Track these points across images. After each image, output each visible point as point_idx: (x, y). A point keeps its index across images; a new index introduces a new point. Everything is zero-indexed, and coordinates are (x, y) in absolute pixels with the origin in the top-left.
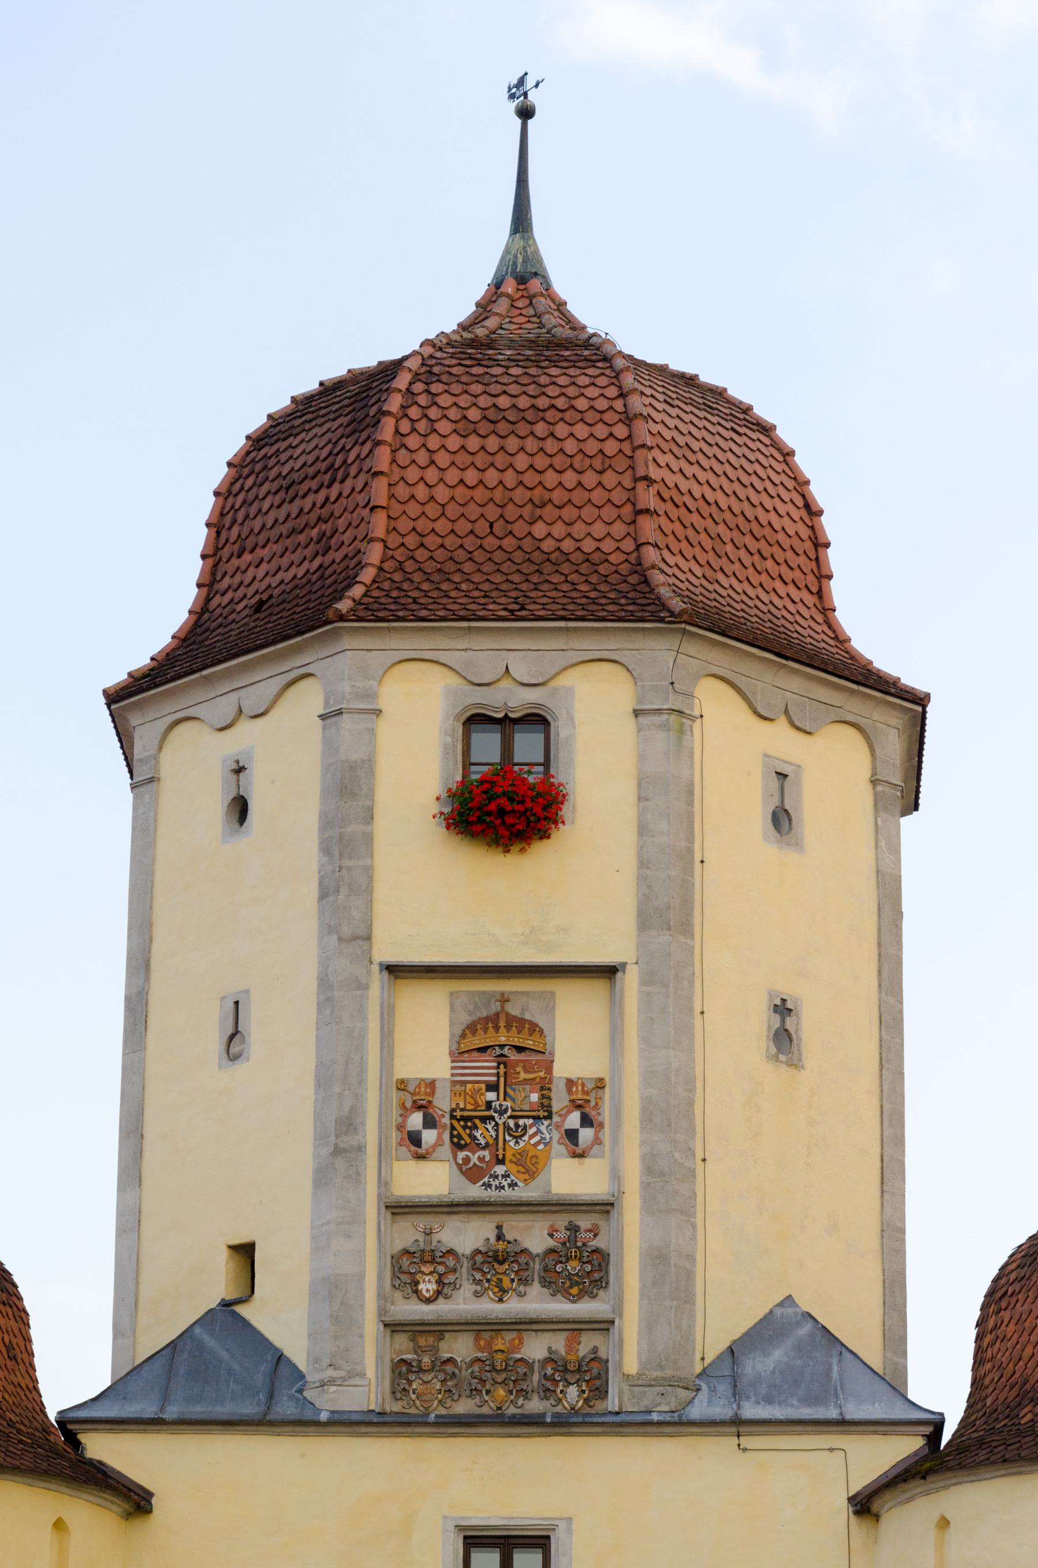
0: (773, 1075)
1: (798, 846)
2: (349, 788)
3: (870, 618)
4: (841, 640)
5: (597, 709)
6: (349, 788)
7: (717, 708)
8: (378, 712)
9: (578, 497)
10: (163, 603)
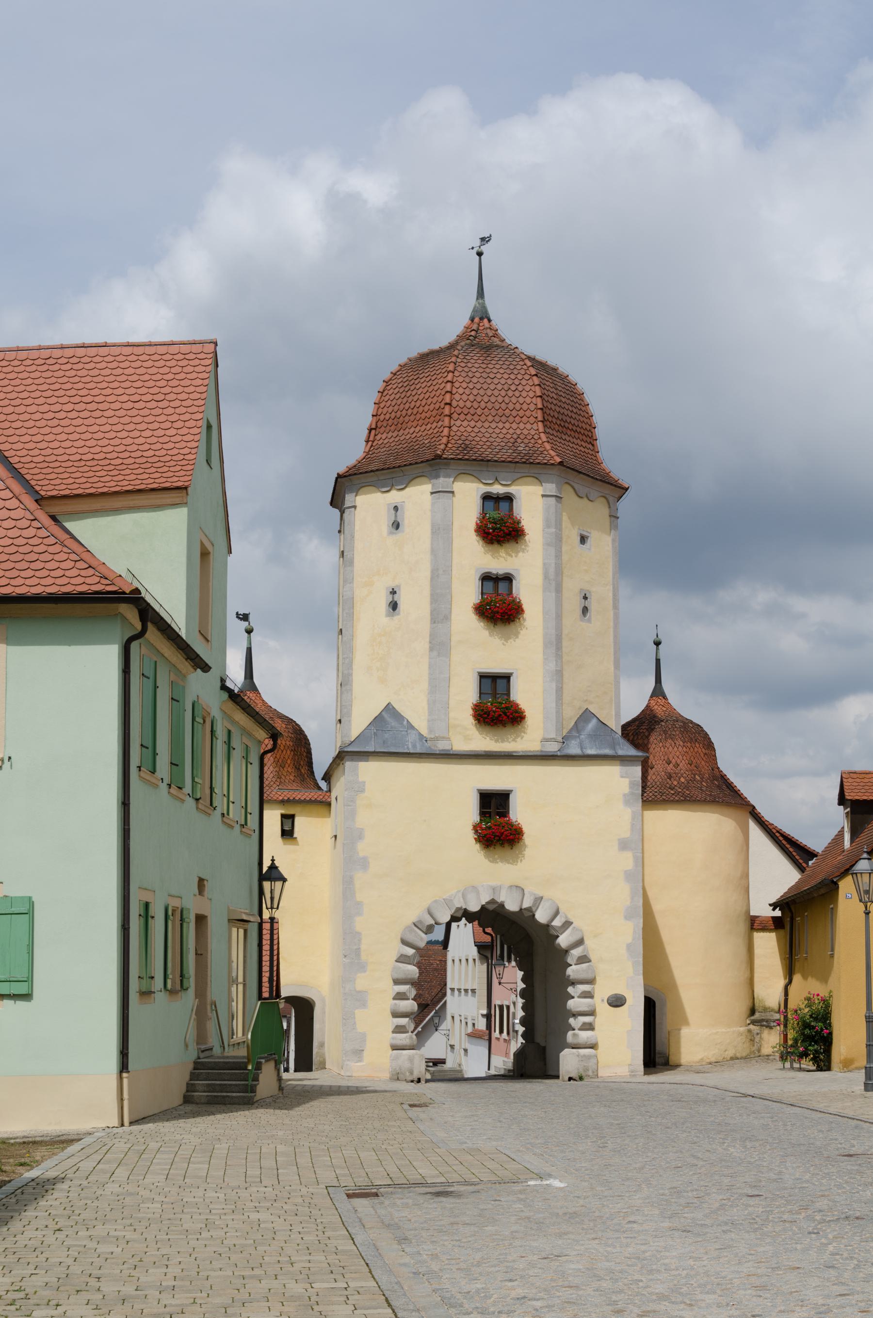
1: (589, 621)
2: (442, 532)
8: (453, 492)
9: (521, 413)
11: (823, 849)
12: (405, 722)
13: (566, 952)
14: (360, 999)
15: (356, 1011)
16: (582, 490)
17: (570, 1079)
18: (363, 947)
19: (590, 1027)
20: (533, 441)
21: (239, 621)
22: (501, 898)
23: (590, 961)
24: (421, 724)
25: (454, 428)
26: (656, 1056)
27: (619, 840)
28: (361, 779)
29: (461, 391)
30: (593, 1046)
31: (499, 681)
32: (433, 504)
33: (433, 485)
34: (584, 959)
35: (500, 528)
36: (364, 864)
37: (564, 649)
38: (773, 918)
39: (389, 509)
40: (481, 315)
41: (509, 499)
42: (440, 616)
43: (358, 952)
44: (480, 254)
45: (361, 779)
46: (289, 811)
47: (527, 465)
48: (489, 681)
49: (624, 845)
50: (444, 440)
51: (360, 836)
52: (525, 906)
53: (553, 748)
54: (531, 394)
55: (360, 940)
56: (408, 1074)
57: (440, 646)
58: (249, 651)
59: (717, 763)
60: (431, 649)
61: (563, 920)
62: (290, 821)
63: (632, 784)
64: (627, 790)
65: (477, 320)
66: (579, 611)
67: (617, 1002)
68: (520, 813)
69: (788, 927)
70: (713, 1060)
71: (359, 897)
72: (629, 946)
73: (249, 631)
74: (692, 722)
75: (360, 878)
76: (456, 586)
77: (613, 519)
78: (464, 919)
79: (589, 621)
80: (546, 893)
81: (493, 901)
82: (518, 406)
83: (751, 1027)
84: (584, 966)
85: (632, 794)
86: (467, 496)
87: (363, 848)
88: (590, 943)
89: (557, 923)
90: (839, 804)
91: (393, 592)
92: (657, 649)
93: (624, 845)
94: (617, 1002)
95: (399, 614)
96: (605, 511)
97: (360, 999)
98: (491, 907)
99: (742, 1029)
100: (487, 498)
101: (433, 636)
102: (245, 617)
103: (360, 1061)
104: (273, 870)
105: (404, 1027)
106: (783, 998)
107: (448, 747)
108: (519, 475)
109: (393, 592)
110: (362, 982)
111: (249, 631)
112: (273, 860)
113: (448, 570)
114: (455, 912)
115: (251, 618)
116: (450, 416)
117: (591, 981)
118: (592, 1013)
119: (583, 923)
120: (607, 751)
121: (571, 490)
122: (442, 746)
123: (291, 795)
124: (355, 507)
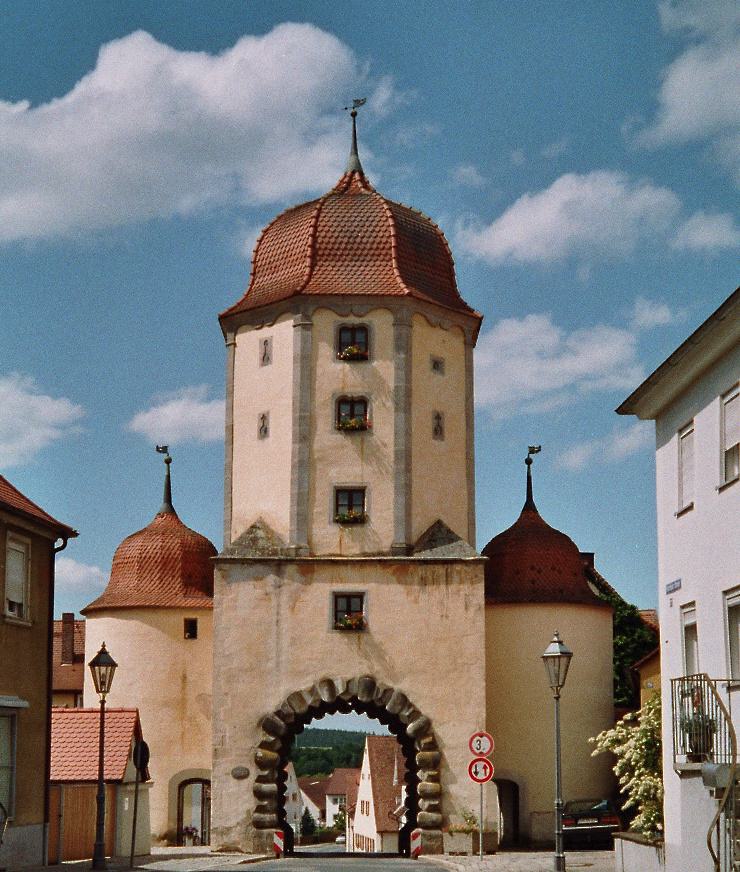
2: (306, 362)
29: (323, 234)
31: (355, 495)
33: (323, 340)
38: (298, 775)
42: (304, 434)
44: (354, 115)
48: (346, 495)
58: (168, 476)
59: (623, 603)
66: (429, 431)
68: (372, 614)
73: (168, 461)
78: (369, 700)
91: (264, 418)
92: (529, 467)
96: (461, 347)
100: (343, 329)
102: (165, 450)
109: (264, 418)
111: (168, 461)
112: (104, 646)
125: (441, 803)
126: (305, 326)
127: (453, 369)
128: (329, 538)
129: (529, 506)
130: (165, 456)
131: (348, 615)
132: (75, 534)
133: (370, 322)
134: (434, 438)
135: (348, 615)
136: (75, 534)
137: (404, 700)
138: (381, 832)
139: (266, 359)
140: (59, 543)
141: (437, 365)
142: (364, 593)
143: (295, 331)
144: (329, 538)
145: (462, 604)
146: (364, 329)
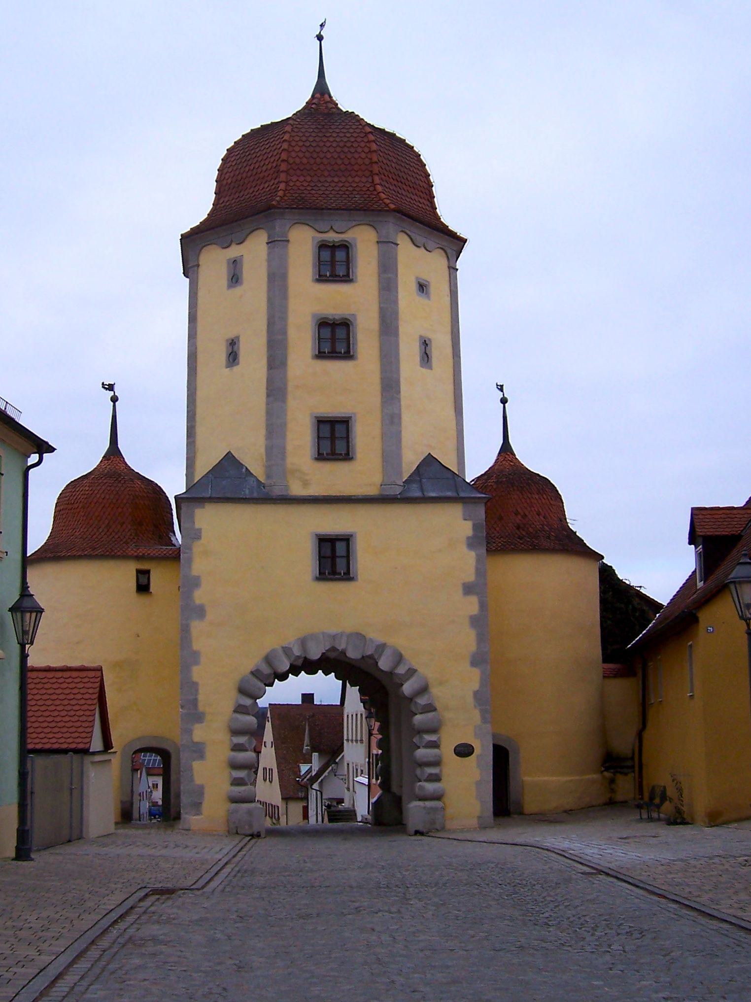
0: (428, 335)
2: (277, 281)
3: (450, 210)
4: (438, 218)
5: (364, 242)
6: (277, 281)
7: (403, 242)
8: (288, 241)
10: (199, 205)
11: (668, 601)
12: (244, 470)
13: (411, 700)
14: (199, 751)
15: (194, 763)
16: (419, 239)
17: (417, 833)
18: (201, 697)
19: (436, 778)
20: (368, 193)
21: (104, 390)
22: (341, 646)
23: (435, 710)
24: (257, 469)
25: (291, 184)
26: (505, 803)
27: (464, 584)
28: (197, 526)
30: (438, 797)
31: (338, 427)
32: (269, 254)
34: (430, 708)
35: (334, 265)
36: (200, 612)
37: (402, 393)
39: (228, 263)
40: (321, 89)
41: (345, 247)
43: (195, 703)
45: (197, 526)
46: (144, 566)
47: (368, 209)
49: (468, 589)
50: (280, 193)
51: (195, 583)
52: (369, 653)
53: (397, 491)
54: (366, 150)
55: (197, 690)
56: (247, 827)
57: (276, 391)
60: (268, 396)
61: (407, 668)
62: (147, 576)
63: (475, 527)
64: (470, 532)
65: (318, 95)
67: (464, 751)
69: (640, 675)
70: (568, 807)
71: (196, 646)
72: (476, 694)
73: (114, 399)
74: (538, 475)
75: (197, 627)
76: (292, 333)
77: (452, 270)
79: (431, 368)
80: (391, 641)
81: (333, 649)
82: (353, 161)
83: (606, 773)
84: (430, 715)
85: (475, 536)
86: (302, 242)
87: (199, 596)
88: (436, 691)
89: (401, 670)
90: (690, 543)
93: (468, 589)
94: (464, 751)
95: (238, 364)
96: (444, 262)
97: (199, 751)
98: (332, 655)
99: (595, 776)
100: (323, 246)
101: (270, 381)
102: (111, 387)
103: (198, 814)
104: (26, 599)
105: (242, 779)
106: (637, 744)
107: (284, 493)
108: (354, 223)
110: (199, 733)
113: (284, 319)
114: (295, 660)
115: (116, 388)
116: (286, 172)
117: (434, 731)
118: (437, 763)
119: (427, 670)
120: (449, 494)
121: (406, 237)
122: (277, 491)
123: (142, 551)
124: (198, 266)
125: (441, 771)
126: (277, 243)
127: (438, 287)
128: (310, 475)
129: (506, 448)
130: (112, 393)
131: (334, 559)
132: (51, 450)
133: (354, 239)
134: (422, 366)
135: (334, 559)
136: (51, 450)
137: (399, 658)
138: (286, 799)
139: (235, 279)
140: (34, 458)
141: (422, 287)
142: (352, 536)
143: (269, 248)
144: (310, 475)
145: (449, 531)
146: (345, 247)
